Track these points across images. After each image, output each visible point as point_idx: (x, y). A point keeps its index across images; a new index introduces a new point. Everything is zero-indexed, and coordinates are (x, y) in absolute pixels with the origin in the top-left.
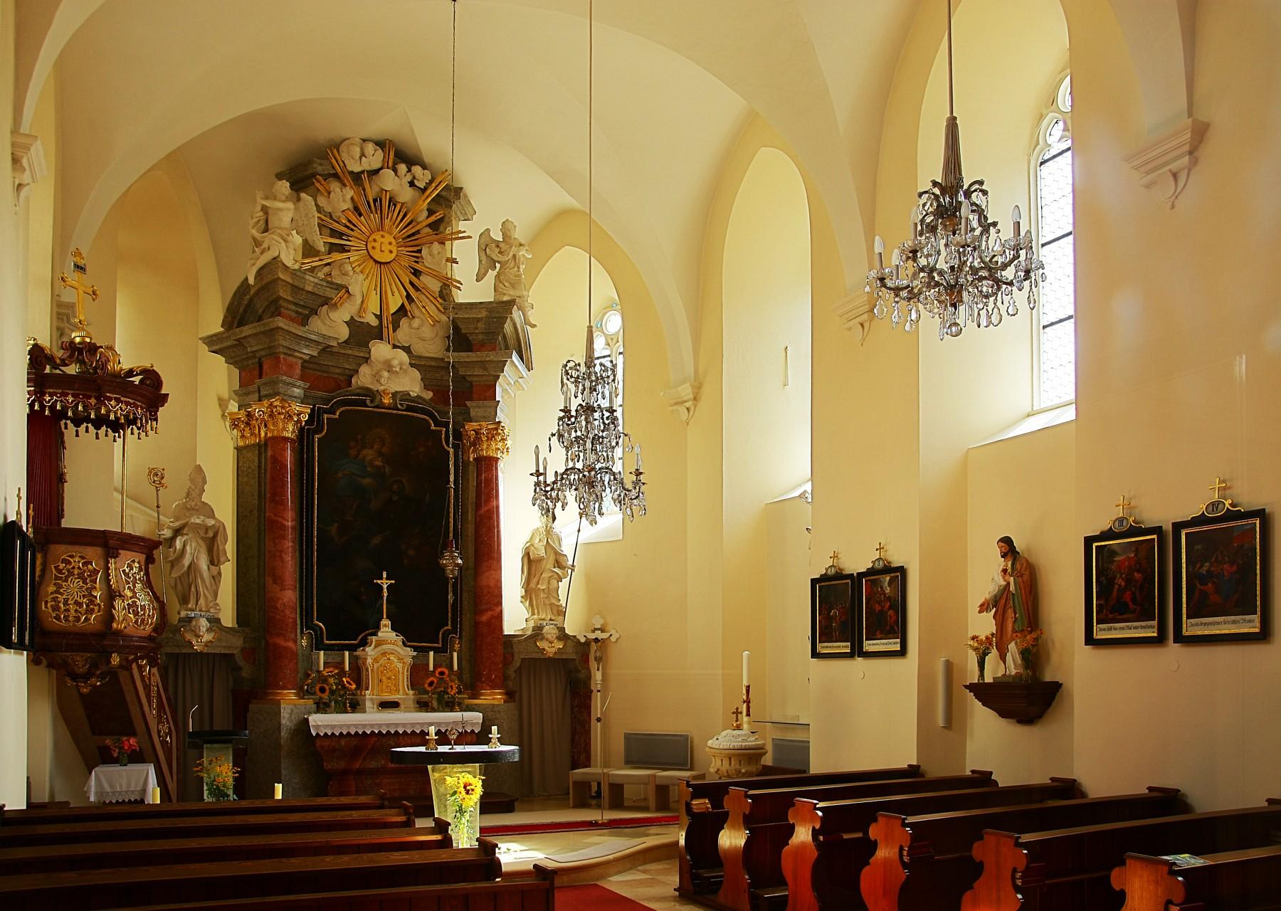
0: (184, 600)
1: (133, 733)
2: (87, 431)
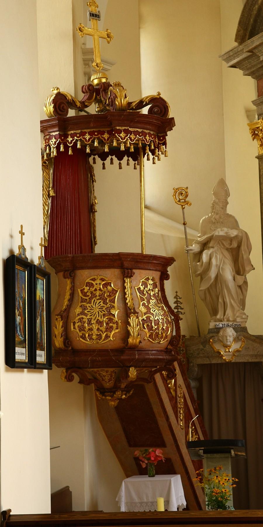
0: (215, 312)
1: (162, 444)
2: (112, 163)
